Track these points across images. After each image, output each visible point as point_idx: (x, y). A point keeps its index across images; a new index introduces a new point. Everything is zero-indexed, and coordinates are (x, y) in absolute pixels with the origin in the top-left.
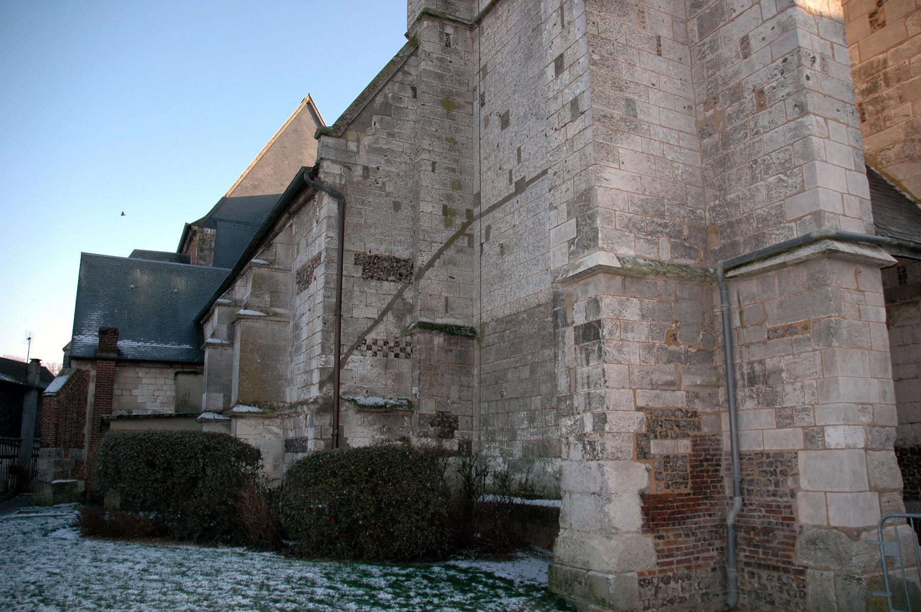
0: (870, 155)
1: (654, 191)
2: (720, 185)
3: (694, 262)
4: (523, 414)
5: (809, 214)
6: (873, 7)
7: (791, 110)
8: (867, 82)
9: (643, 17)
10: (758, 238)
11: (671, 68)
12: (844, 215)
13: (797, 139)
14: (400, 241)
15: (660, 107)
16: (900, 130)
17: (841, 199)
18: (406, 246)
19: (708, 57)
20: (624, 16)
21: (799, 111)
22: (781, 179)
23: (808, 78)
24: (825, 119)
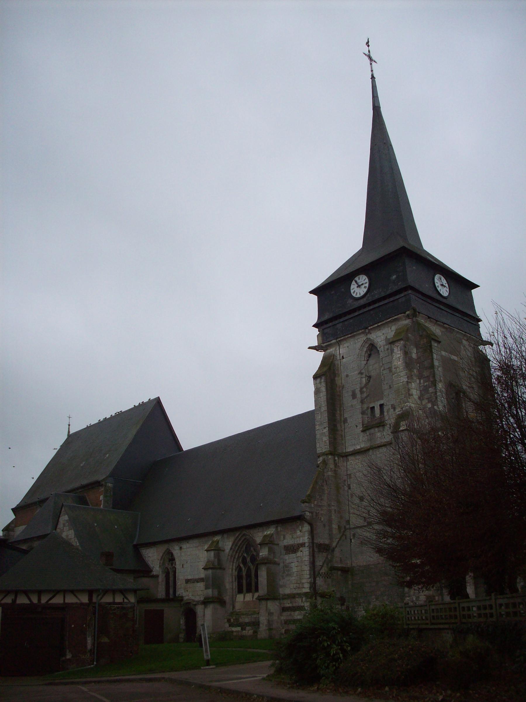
4: (373, 597)
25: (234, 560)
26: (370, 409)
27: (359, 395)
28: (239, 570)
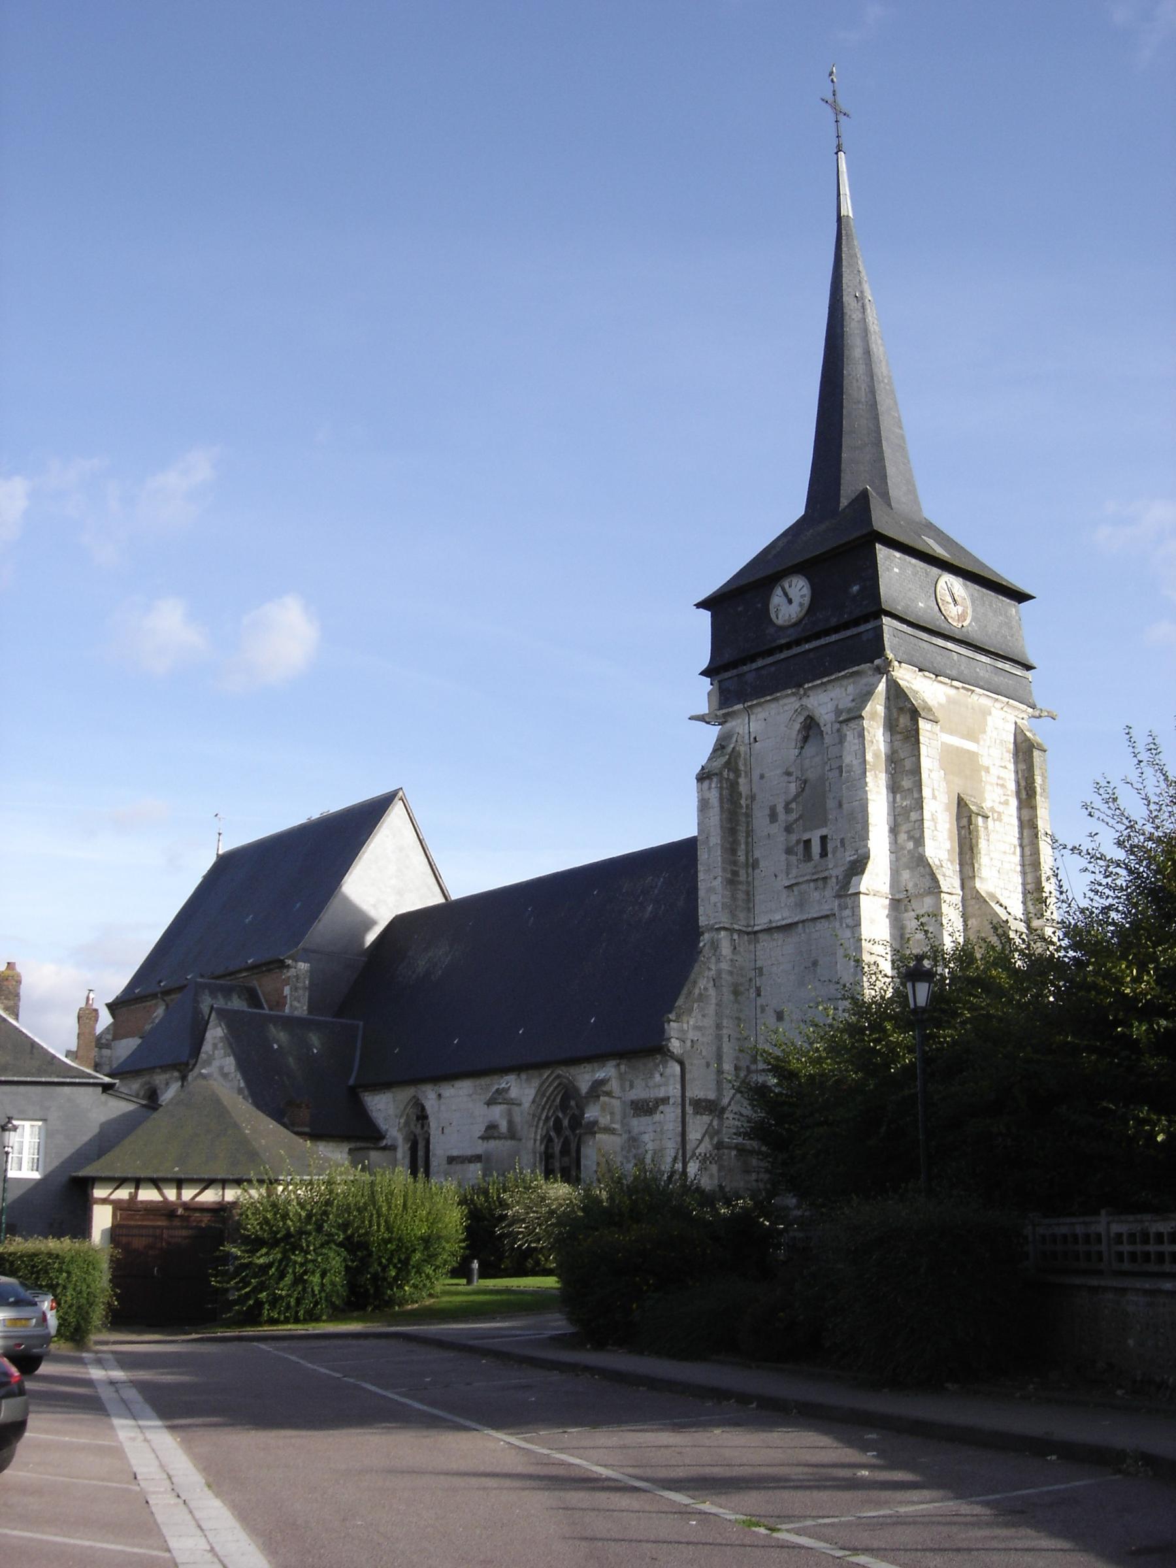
25: (538, 1123)
26: (802, 844)
27: (782, 816)
28: (548, 1140)
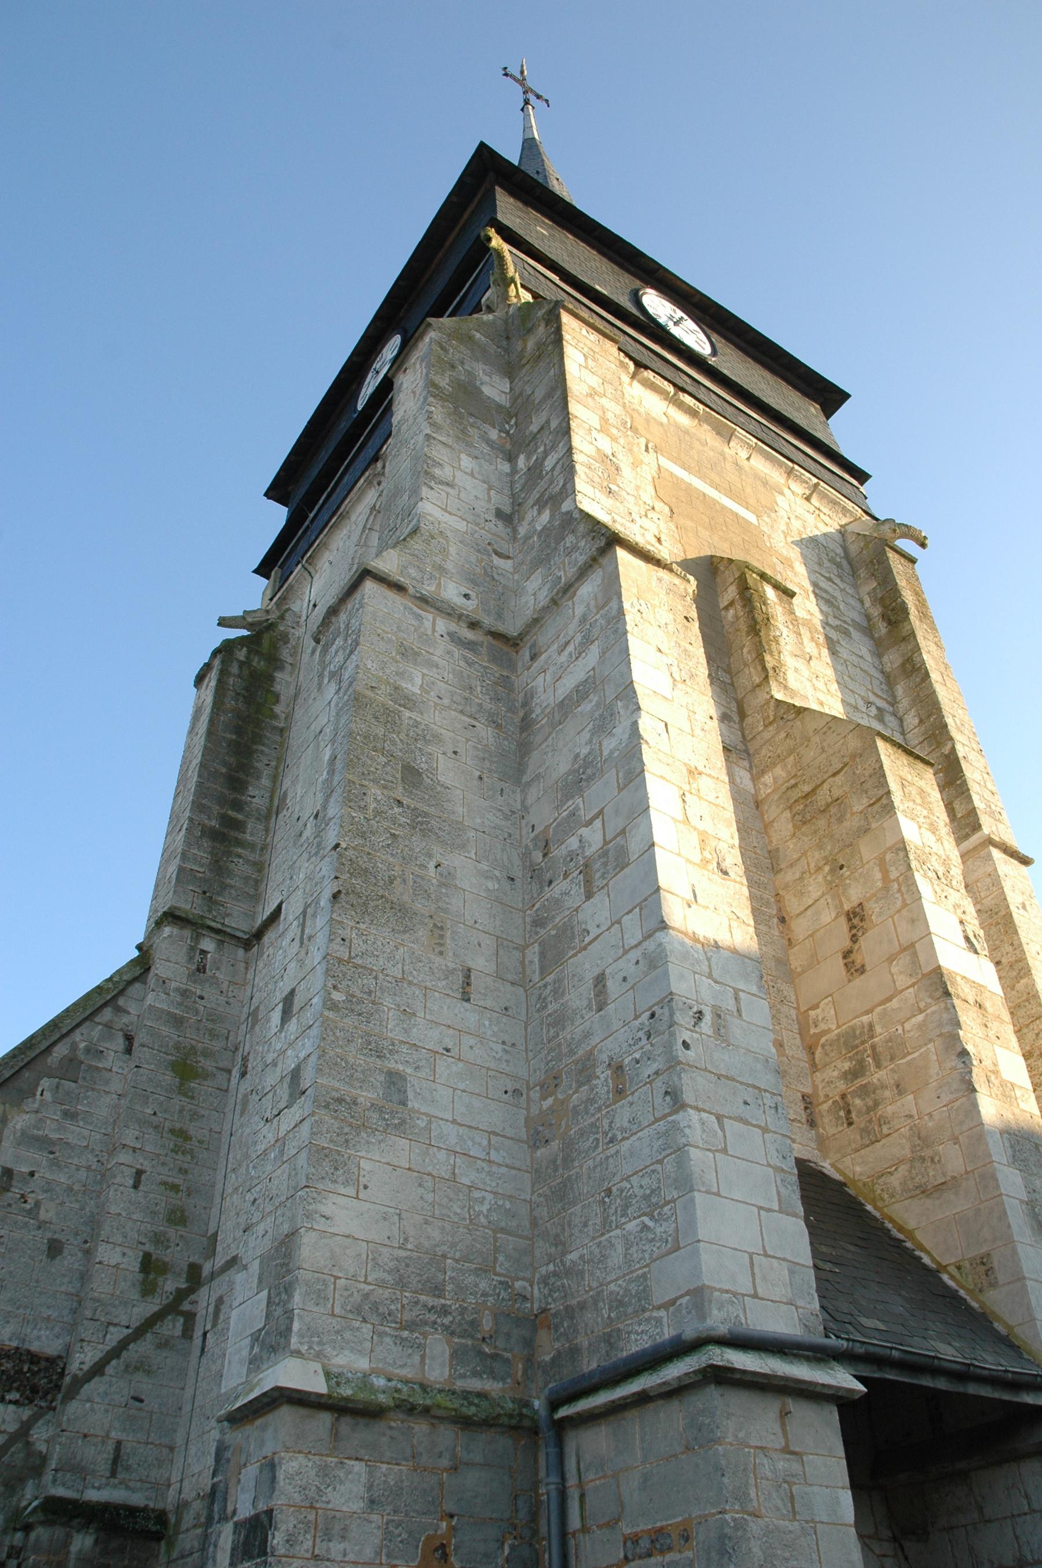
0: (864, 1184)
1: (426, 1244)
2: (557, 1235)
3: (500, 1385)
5: (687, 1293)
6: (847, 943)
7: (661, 1100)
8: (851, 1059)
9: (442, 937)
10: (610, 1340)
11: (487, 1023)
12: (755, 1296)
13: (668, 1151)
14: (48, 1319)
15: (455, 1089)
16: (904, 1141)
17: (748, 1263)
18: (57, 1329)
19: (550, 1006)
20: (405, 932)
21: (671, 1103)
22: (645, 1227)
23: (686, 1045)
24: (719, 1118)
